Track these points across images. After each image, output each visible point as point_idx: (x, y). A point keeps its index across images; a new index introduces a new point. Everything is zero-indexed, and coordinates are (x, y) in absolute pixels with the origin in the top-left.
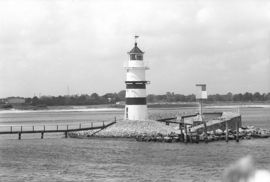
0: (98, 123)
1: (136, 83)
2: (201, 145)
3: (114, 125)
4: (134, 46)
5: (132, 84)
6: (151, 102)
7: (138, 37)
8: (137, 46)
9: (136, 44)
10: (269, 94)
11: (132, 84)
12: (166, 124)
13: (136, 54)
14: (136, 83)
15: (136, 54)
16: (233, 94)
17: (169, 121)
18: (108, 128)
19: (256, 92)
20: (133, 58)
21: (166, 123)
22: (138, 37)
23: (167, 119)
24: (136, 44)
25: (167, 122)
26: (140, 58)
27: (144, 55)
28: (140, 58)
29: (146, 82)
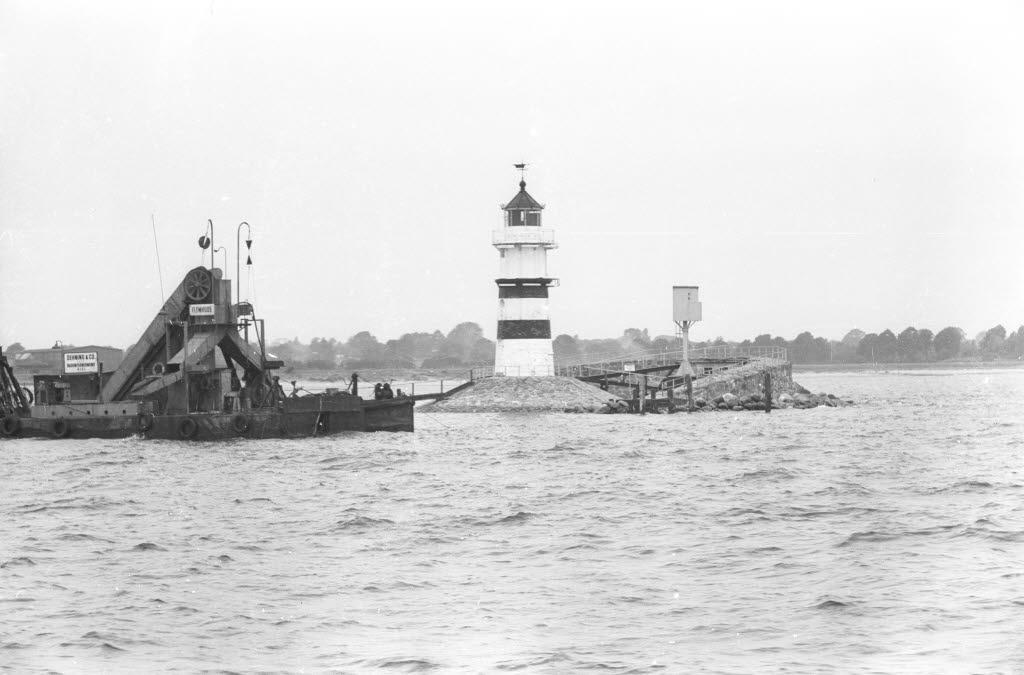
0: (986, 380)
1: (524, 285)
2: (209, 446)
3: (470, 390)
4: (519, 189)
5: (514, 285)
6: (189, 328)
7: (517, 166)
8: (527, 189)
9: (523, 185)
10: (1021, 329)
11: (514, 285)
12: (601, 388)
13: (523, 209)
14: (524, 285)
15: (523, 209)
16: (935, 333)
17: (609, 379)
18: (453, 397)
19: (947, 326)
20: (514, 220)
21: (602, 384)
22: (517, 166)
23: (603, 377)
24: (523, 185)
25: (603, 383)
26: (534, 220)
27: (544, 215)
28: (534, 220)
29: (549, 281)
